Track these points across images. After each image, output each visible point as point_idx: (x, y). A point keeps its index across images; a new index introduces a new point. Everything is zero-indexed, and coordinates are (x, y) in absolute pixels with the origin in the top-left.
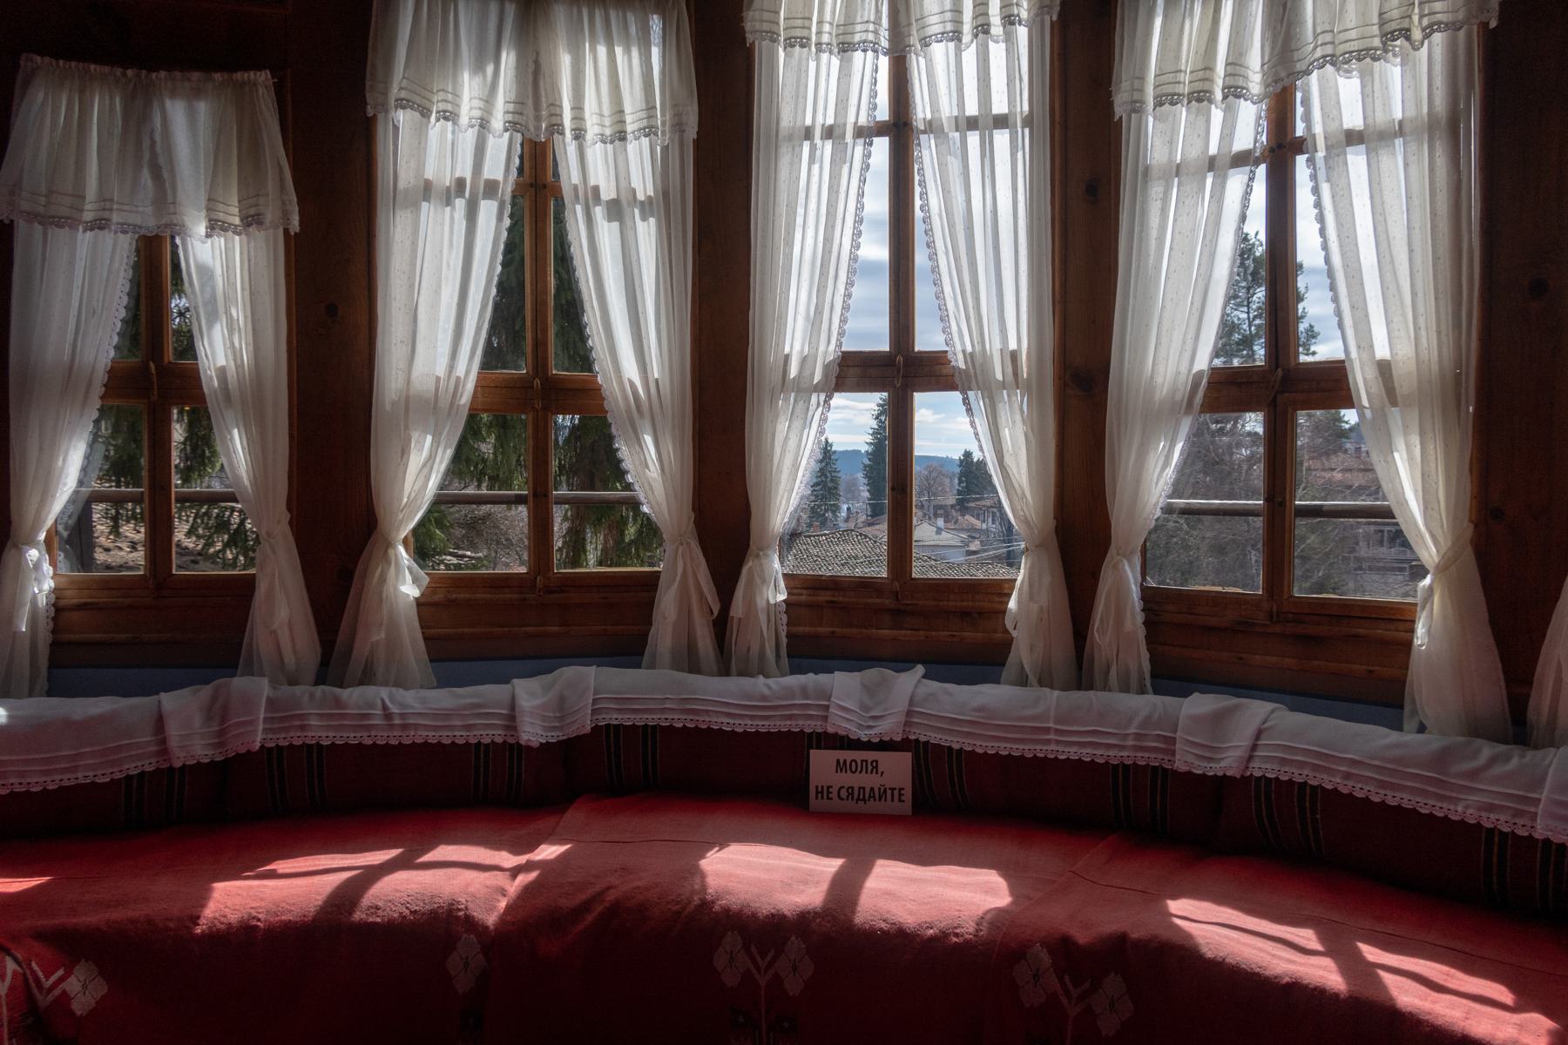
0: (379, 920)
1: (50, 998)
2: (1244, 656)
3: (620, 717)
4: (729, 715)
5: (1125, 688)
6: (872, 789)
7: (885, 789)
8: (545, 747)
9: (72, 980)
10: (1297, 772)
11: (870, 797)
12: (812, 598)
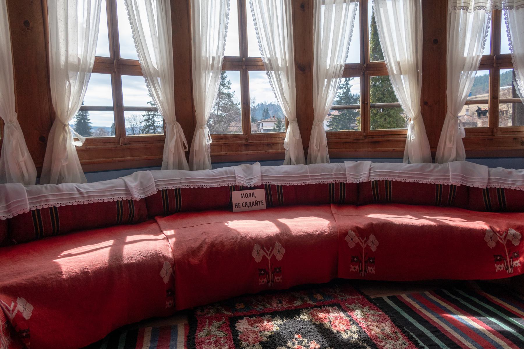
0: (134, 261)
1: (14, 314)
2: (357, 149)
3: (166, 187)
4: (204, 182)
5: (322, 162)
6: (253, 202)
7: (257, 202)
8: (141, 200)
9: (18, 306)
10: (385, 178)
11: (253, 205)
12: (218, 142)
